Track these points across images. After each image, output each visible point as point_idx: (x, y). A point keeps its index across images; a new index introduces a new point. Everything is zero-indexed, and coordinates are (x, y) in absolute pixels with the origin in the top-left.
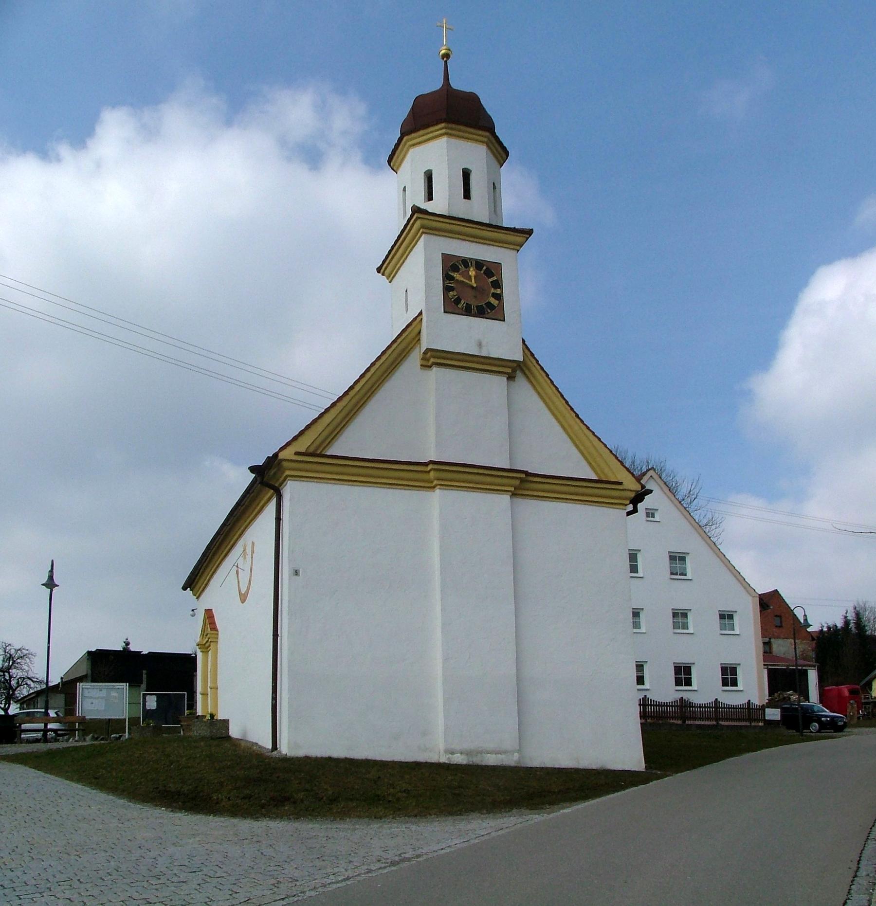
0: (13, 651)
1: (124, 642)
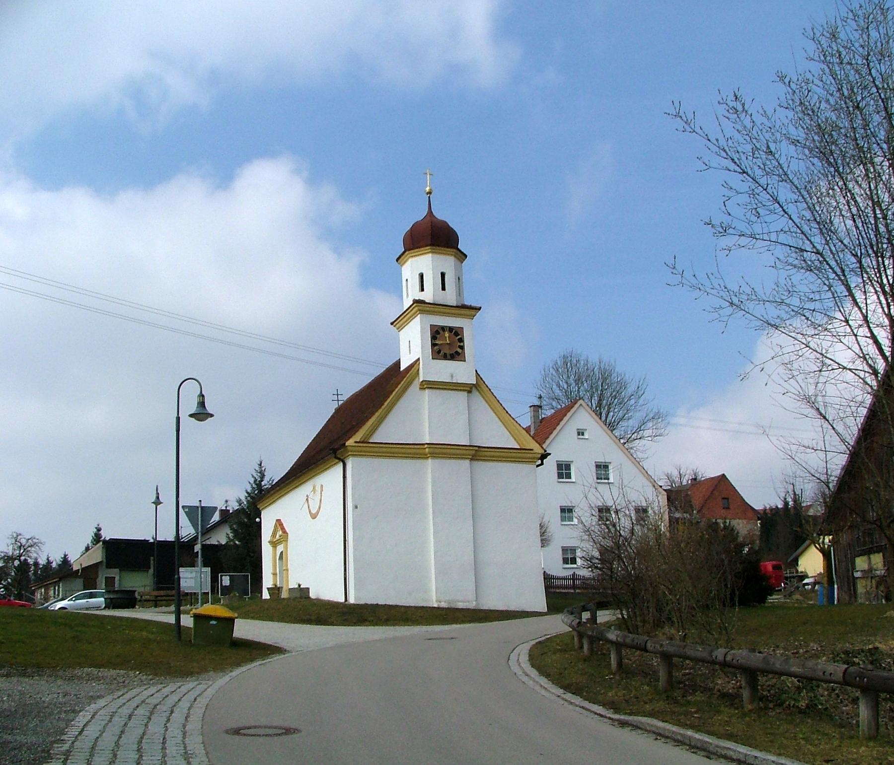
0: (23, 541)
1: (96, 528)
